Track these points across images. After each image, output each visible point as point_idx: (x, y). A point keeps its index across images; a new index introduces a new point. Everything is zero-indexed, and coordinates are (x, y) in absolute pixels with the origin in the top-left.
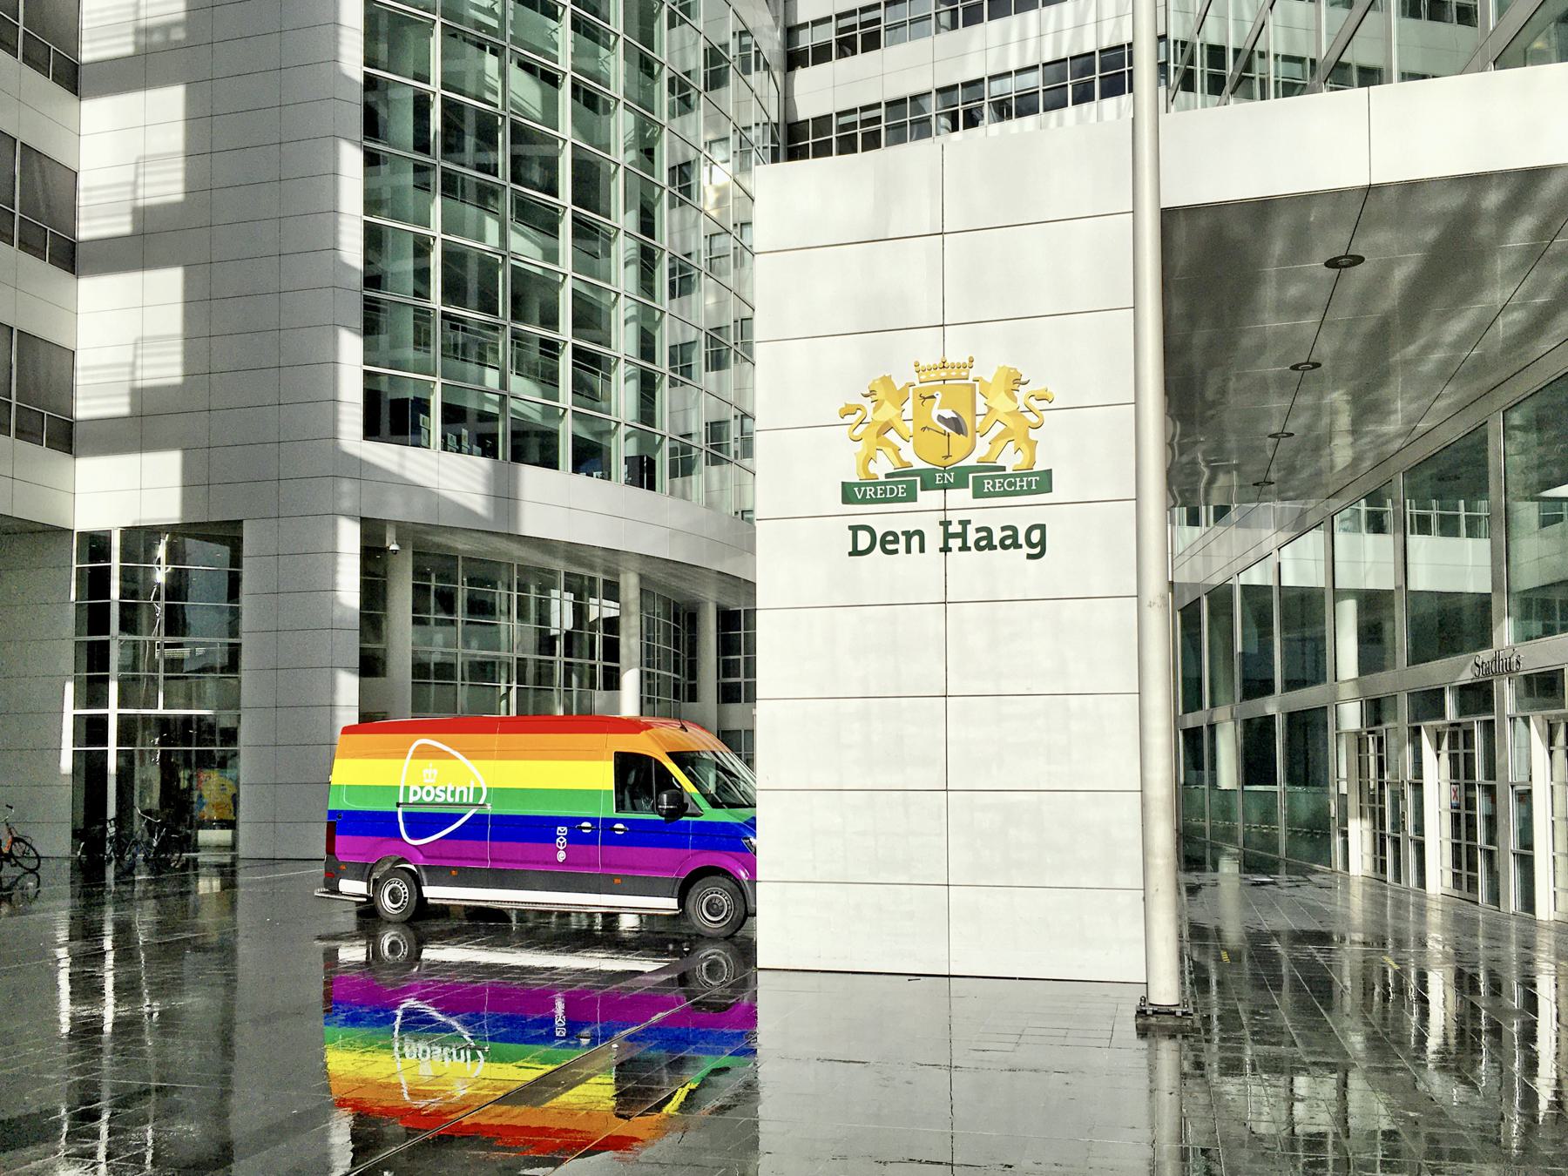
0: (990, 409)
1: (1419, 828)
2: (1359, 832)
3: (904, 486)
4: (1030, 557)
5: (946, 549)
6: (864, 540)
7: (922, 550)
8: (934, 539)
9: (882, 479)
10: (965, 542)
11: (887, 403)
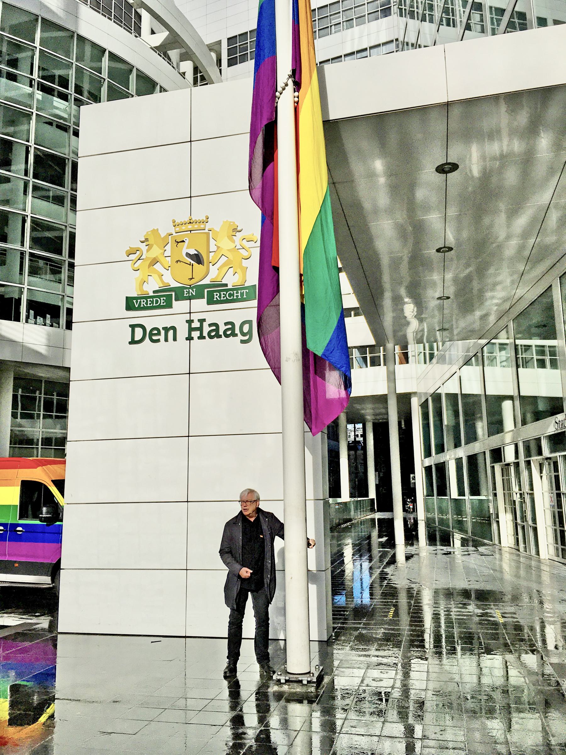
0: (218, 247)
1: (534, 520)
2: (506, 521)
3: (165, 298)
4: (243, 342)
5: (190, 338)
6: (139, 333)
7: (175, 339)
8: (183, 332)
9: (151, 294)
10: (201, 333)
11: (155, 246)
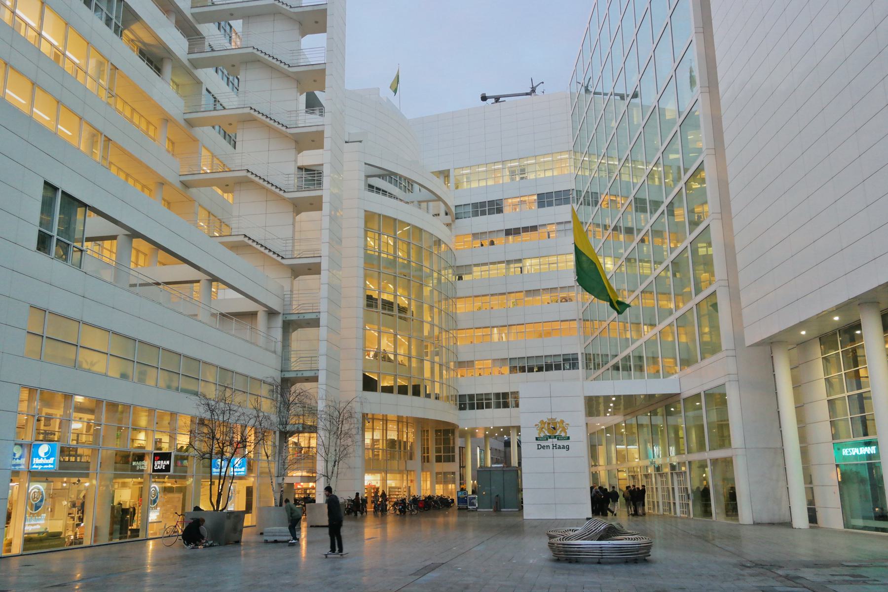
3: (546, 438)
8: (551, 447)
